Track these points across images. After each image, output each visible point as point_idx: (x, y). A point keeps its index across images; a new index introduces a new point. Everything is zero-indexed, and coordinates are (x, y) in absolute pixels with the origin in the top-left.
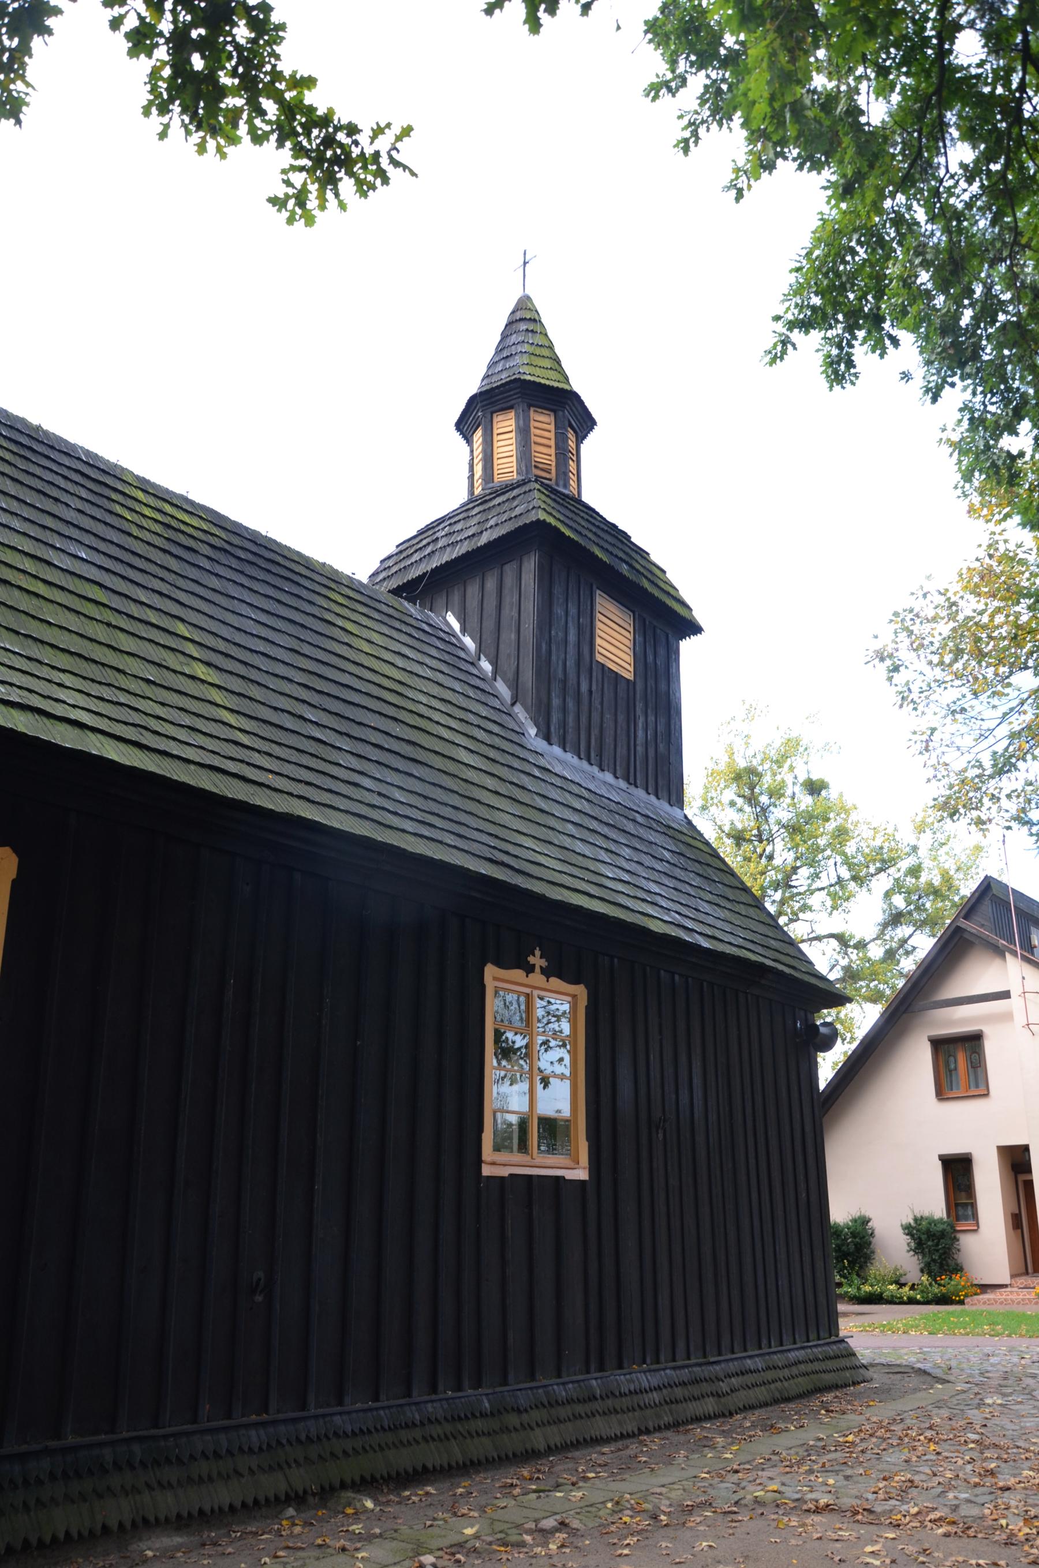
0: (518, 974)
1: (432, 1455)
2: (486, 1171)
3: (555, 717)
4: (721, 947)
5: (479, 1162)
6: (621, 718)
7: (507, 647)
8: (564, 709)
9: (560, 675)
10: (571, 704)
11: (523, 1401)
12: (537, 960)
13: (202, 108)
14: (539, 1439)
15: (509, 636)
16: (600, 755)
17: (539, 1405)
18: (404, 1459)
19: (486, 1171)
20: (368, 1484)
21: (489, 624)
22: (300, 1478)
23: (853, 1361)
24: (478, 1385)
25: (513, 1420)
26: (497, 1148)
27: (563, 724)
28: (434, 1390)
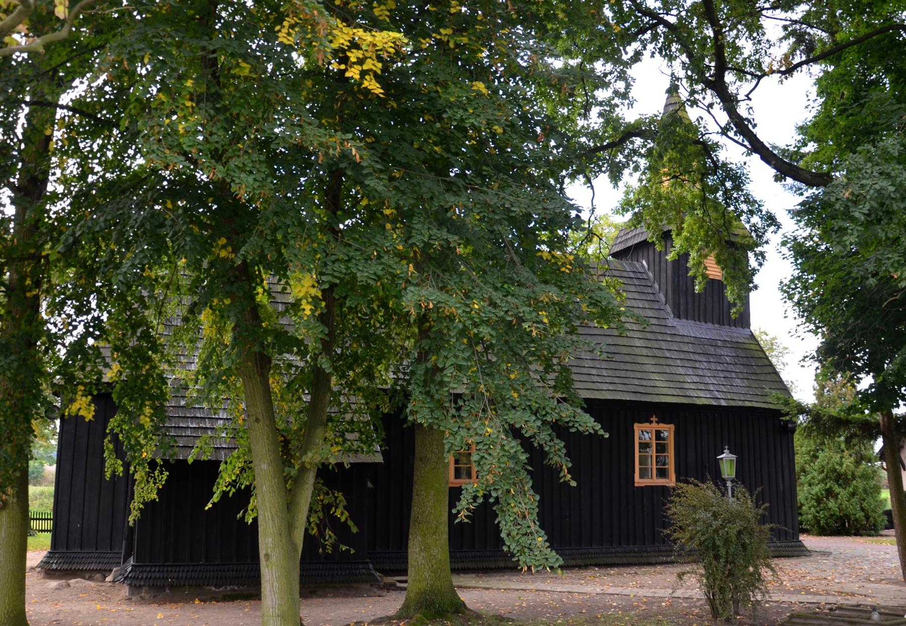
0: (647, 424)
1: (617, 561)
2: (636, 485)
3: (682, 308)
4: (732, 403)
5: (634, 482)
6: (716, 298)
7: (663, 280)
8: (687, 304)
9: (684, 289)
10: (690, 300)
11: (649, 549)
12: (654, 419)
13: (348, 551)
14: (653, 560)
15: (663, 275)
16: (705, 317)
17: (655, 551)
18: (609, 561)
19: (636, 485)
20: (599, 565)
21: (657, 268)
22: (579, 562)
23: (803, 549)
24: (635, 544)
25: (645, 554)
26: (641, 477)
27: (687, 309)
28: (620, 544)
